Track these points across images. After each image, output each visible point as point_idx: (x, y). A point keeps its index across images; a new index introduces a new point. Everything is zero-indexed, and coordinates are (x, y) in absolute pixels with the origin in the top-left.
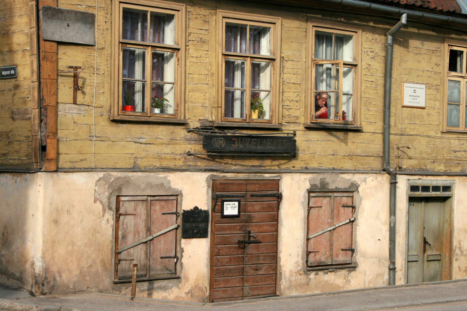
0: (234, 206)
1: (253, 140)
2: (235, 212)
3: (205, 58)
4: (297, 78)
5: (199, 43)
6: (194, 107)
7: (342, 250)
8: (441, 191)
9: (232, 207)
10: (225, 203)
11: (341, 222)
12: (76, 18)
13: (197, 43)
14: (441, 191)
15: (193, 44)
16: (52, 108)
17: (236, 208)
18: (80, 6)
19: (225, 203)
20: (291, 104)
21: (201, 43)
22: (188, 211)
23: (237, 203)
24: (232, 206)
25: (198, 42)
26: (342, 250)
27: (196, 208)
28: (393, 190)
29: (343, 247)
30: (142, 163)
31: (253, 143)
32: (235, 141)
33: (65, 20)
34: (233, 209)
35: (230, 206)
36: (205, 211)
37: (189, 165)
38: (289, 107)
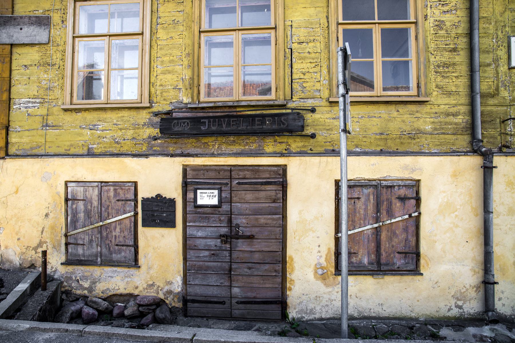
0: (212, 195)
1: (232, 120)
2: (215, 201)
3: (178, 40)
4: (315, 47)
5: (170, 26)
6: (164, 90)
7: (398, 253)
8: (116, 18)
9: (210, 196)
10: (199, 191)
11: (395, 218)
12: (30, 22)
13: (167, 26)
14: (116, 18)
15: (163, 28)
16: (4, 103)
17: (215, 197)
18: (37, 12)
19: (199, 191)
20: (306, 77)
21: (174, 25)
22: (148, 199)
23: (216, 192)
24: (209, 195)
25: (168, 25)
26: (398, 253)
27: (158, 196)
28: (389, 103)
29: (399, 250)
30: (96, 148)
31: (257, 123)
32: (205, 123)
33: (18, 25)
34: (211, 198)
35: (206, 194)
36: (170, 199)
37: (155, 151)
38: (303, 80)
